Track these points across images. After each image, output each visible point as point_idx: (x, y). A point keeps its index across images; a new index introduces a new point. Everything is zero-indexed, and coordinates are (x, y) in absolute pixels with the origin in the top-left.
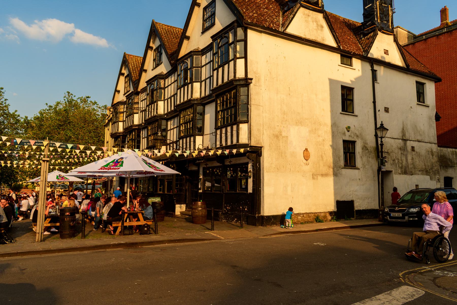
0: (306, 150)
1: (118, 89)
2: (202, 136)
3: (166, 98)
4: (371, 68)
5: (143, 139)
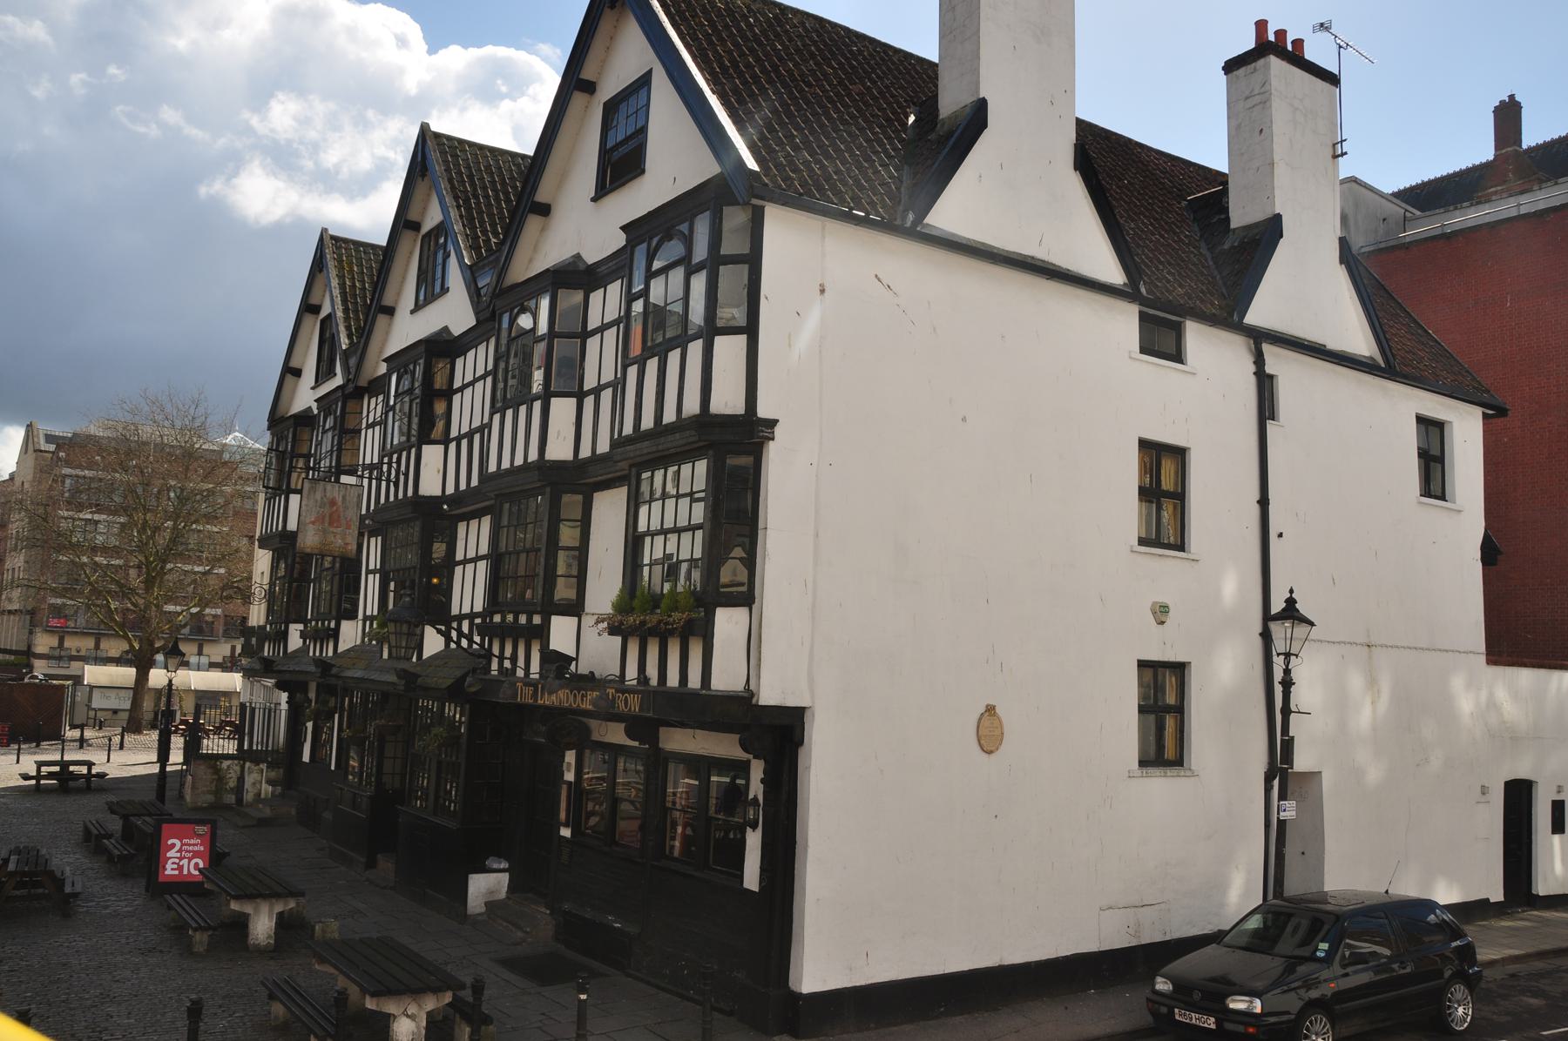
0: (990, 709)
1: (294, 363)
2: (576, 619)
3: (454, 433)
4: (1252, 368)
5: (371, 577)
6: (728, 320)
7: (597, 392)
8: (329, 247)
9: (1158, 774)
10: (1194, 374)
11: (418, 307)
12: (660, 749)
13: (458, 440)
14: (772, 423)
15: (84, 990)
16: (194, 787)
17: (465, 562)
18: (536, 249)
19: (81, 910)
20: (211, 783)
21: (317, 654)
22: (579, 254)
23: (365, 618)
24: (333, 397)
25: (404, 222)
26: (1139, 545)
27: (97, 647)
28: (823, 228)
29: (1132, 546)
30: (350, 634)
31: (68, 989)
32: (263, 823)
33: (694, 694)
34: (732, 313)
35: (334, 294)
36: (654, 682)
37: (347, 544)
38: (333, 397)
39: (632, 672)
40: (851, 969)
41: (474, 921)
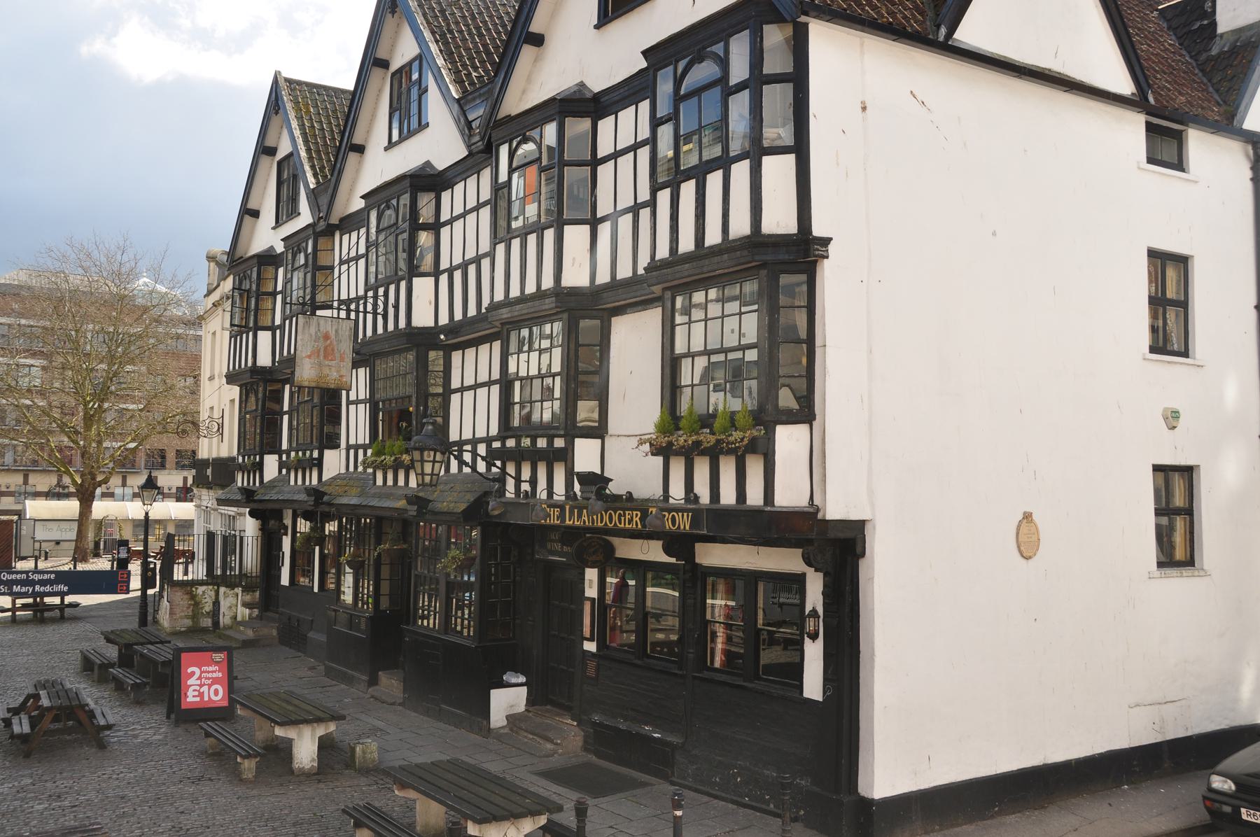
0: (1028, 517)
1: (252, 205)
2: (599, 441)
3: (444, 264)
5: (352, 407)
6: (773, 140)
7: (613, 217)
8: (284, 90)
9: (1175, 574)
10: (1196, 182)
11: (391, 145)
12: (697, 564)
13: (450, 272)
14: (826, 242)
15: (155, 824)
16: (172, 613)
17: (462, 389)
18: (529, 80)
19: (112, 740)
20: (188, 608)
21: (245, 484)
22: (582, 82)
23: (348, 448)
24: (302, 235)
25: (373, 61)
26: (1150, 352)
27: (26, 482)
28: (862, 45)
29: (1144, 354)
30: (334, 463)
31: (139, 823)
32: (247, 644)
33: (756, 512)
34: (778, 131)
35: (296, 135)
36: (705, 498)
37: (341, 376)
38: (302, 235)
39: (677, 492)
40: (916, 774)
41: (496, 735)
